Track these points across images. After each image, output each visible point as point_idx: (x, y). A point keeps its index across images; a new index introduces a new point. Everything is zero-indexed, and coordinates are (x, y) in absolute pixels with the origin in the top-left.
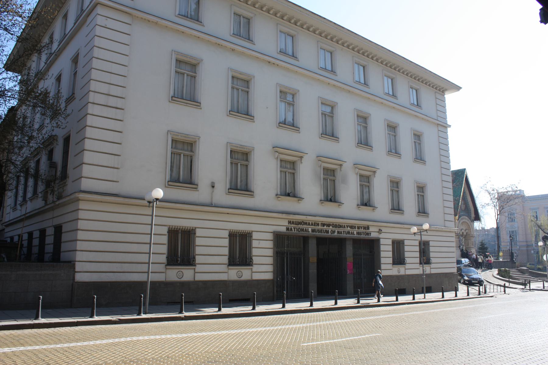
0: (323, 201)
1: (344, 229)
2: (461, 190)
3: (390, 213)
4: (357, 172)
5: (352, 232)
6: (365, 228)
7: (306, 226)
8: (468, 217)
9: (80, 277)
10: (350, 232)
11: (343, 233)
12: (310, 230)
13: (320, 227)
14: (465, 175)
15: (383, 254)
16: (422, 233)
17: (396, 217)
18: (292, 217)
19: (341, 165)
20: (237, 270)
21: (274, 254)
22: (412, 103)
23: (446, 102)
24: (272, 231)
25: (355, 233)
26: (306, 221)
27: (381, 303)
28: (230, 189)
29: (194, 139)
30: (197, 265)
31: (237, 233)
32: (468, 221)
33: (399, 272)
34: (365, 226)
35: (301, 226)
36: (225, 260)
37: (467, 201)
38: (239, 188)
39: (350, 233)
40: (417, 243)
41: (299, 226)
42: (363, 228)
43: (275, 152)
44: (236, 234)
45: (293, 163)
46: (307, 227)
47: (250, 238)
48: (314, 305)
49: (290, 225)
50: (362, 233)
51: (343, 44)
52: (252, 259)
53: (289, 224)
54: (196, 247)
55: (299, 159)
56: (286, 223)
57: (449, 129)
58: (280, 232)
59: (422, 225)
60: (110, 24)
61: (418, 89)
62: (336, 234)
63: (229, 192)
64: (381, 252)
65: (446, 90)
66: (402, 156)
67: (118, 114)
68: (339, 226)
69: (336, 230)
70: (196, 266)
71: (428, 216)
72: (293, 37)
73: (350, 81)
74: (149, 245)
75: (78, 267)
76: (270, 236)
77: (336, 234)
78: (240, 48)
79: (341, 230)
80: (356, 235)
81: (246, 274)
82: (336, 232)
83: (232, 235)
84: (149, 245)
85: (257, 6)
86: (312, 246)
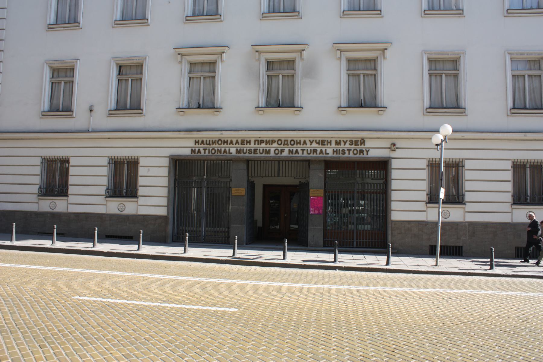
7: (225, 145)
18: (196, 135)
24: (168, 155)
27: (391, 267)
29: (71, 63)
35: (216, 146)
36: (508, 197)
41: (214, 146)
44: (124, 161)
53: (195, 144)
55: (381, 54)
56: (191, 144)
70: (466, 204)
76: (165, 162)
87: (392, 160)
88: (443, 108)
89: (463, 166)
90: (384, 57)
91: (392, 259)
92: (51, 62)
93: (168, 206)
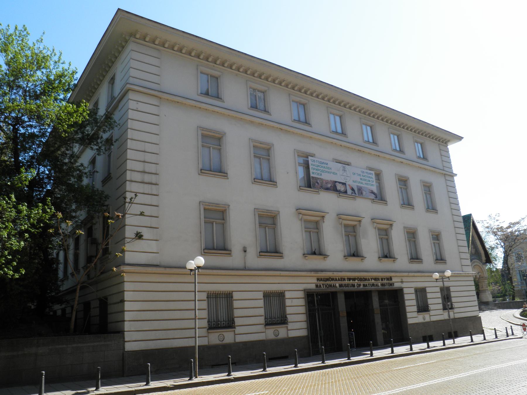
0: (306, 254)
1: (369, 281)
2: (470, 235)
3: (409, 263)
4: (375, 226)
5: (376, 284)
6: (388, 279)
7: (333, 282)
8: (479, 260)
9: (129, 347)
10: (374, 284)
11: (368, 285)
12: (337, 285)
13: (346, 282)
14: (472, 220)
15: (407, 303)
16: (444, 280)
17: (415, 266)
19: (360, 221)
20: (274, 330)
21: (306, 311)
22: (394, 149)
23: (450, 152)
24: (303, 289)
25: (379, 284)
26: (333, 277)
28: (261, 252)
29: (224, 207)
30: (236, 327)
31: (267, 294)
32: (480, 265)
33: (424, 319)
34: (388, 277)
37: (477, 244)
38: (269, 251)
39: (375, 285)
40: (438, 289)
41: (327, 282)
42: (386, 279)
43: (299, 213)
45: (354, 227)
46: (334, 283)
47: (231, 298)
48: (374, 355)
49: (318, 282)
50: (386, 285)
51: (350, 108)
52: (287, 318)
53: (317, 281)
54: (234, 310)
55: (321, 219)
56: (315, 281)
57: (455, 178)
58: (310, 289)
59: (444, 272)
60: (141, 107)
61: (422, 143)
62: (362, 287)
63: (260, 255)
64: (406, 301)
65: (449, 141)
66: (415, 208)
67: (153, 189)
68: (364, 280)
69: (362, 284)
71: (445, 263)
72: (304, 106)
73: (360, 142)
74: (194, 311)
75: (128, 336)
76: (301, 294)
77: (362, 287)
78: (368, 150)
79: (366, 282)
80: (380, 287)
81: (282, 332)
82: (362, 285)
83: (267, 296)
84: (194, 311)
85: (226, 65)
86: (341, 301)
87: (427, 288)
88: (214, 249)
89: (232, 297)
90: (324, 222)
91: (395, 349)
92: (207, 204)
93: (307, 328)
